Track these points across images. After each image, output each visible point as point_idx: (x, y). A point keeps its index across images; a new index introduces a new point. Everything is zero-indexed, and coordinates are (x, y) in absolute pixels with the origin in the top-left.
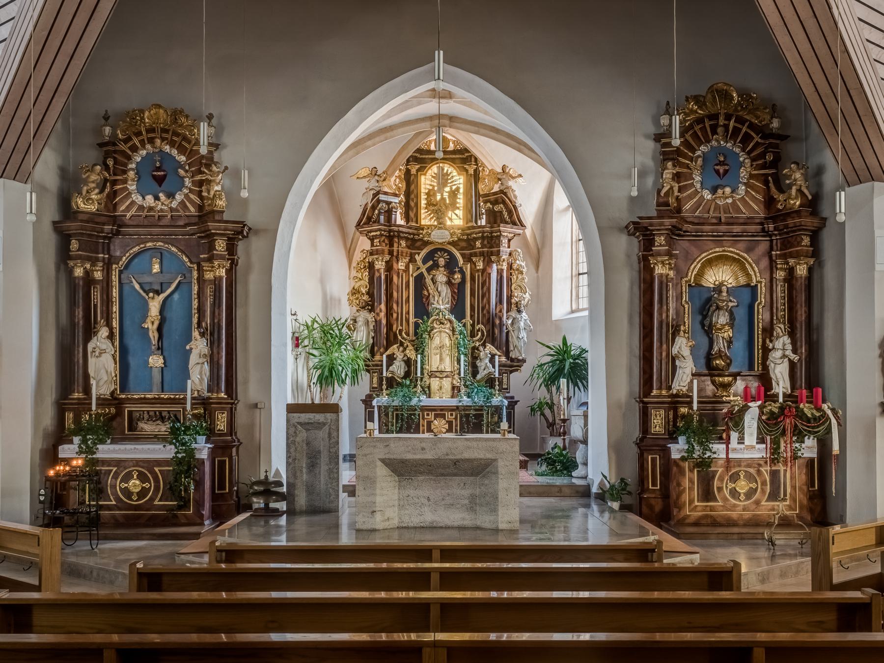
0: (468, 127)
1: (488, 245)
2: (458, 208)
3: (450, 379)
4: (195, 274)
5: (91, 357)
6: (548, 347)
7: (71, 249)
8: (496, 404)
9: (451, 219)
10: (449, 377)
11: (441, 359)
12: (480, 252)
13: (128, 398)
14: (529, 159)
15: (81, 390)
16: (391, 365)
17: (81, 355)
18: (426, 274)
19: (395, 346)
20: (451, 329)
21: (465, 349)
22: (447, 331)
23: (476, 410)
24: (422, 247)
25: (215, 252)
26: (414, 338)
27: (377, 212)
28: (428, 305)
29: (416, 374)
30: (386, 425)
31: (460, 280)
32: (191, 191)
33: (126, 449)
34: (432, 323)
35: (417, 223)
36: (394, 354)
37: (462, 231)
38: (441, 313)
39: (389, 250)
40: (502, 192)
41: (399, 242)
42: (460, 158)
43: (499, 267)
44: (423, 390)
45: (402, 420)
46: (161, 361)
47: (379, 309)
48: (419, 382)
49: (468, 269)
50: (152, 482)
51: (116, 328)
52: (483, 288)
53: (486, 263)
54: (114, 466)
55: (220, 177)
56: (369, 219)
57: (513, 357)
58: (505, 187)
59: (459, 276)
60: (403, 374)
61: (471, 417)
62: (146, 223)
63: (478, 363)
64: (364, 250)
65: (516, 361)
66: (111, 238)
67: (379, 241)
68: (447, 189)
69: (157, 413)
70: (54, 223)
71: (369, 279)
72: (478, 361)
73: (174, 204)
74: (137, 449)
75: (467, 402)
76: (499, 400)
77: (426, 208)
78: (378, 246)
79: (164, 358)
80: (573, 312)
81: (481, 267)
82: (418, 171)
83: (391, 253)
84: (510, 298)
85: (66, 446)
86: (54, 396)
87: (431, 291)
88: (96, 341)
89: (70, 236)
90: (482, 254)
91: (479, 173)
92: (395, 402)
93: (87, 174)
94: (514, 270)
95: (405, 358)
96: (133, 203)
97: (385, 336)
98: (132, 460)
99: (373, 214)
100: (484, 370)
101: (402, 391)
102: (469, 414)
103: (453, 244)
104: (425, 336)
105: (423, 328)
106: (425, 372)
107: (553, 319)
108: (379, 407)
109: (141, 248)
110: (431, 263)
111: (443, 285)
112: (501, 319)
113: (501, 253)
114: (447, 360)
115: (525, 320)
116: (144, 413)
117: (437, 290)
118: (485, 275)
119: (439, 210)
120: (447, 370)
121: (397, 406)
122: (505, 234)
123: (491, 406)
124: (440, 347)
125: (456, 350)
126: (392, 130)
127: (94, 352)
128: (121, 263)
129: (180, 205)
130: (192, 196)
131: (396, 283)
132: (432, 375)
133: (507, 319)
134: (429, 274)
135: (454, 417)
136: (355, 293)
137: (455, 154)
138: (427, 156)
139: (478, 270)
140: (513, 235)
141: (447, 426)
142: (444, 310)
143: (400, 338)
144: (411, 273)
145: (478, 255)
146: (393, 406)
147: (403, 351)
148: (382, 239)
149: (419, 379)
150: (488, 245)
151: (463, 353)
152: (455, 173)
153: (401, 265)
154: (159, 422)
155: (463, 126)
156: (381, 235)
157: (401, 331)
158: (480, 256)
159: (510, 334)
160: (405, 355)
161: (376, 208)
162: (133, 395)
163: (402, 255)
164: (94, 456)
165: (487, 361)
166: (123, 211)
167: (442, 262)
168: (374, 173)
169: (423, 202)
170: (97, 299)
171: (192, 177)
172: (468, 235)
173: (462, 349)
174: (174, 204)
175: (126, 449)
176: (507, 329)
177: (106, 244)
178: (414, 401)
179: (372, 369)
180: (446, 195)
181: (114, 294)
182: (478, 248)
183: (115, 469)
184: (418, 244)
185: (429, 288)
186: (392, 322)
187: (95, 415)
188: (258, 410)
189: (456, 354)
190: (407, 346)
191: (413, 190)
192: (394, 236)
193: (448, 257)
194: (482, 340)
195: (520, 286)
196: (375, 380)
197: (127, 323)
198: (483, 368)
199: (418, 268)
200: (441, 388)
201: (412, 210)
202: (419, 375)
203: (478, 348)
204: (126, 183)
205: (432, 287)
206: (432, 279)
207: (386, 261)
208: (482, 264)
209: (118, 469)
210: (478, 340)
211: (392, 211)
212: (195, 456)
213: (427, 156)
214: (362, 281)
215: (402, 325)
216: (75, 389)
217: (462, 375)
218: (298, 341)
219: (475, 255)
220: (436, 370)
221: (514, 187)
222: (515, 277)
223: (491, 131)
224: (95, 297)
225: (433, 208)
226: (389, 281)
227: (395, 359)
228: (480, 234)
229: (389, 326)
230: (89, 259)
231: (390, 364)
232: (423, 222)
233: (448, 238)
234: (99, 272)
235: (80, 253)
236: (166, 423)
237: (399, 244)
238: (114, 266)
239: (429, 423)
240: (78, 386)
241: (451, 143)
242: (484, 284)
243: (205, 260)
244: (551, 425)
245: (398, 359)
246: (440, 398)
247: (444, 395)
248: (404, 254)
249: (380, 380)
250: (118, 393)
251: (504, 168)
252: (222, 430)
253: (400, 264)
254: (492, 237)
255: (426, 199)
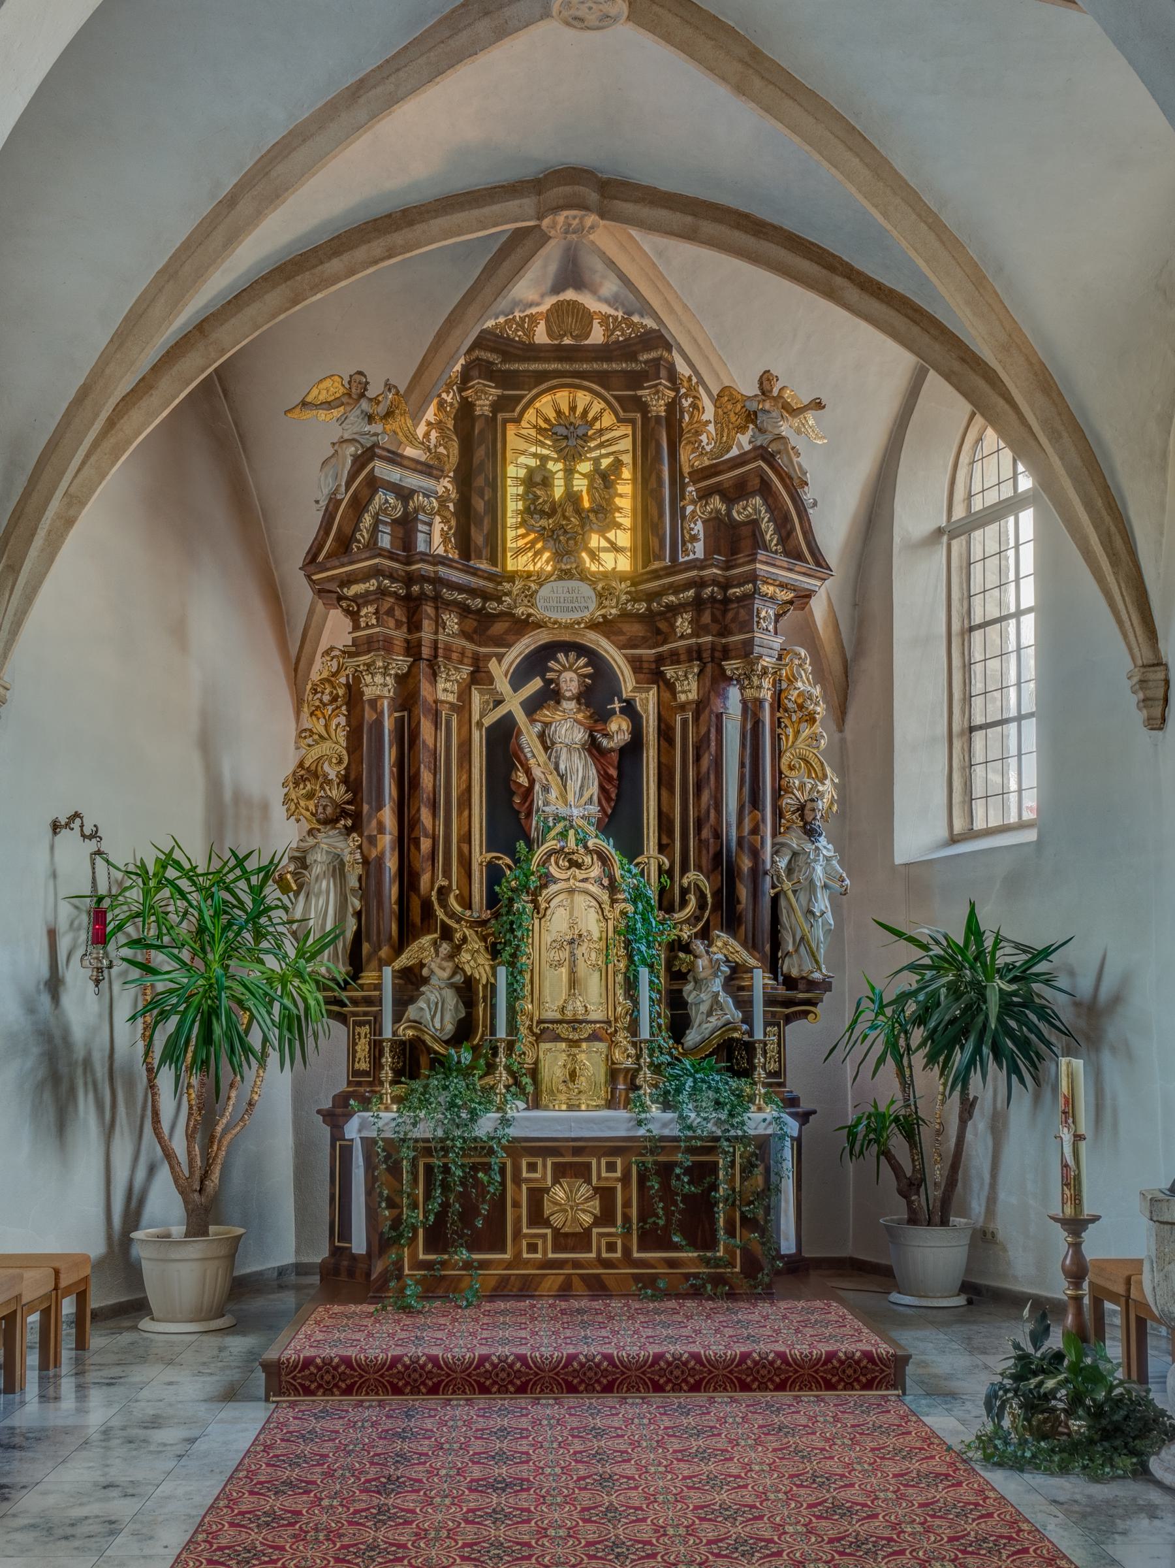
0: (662, 214)
1: (715, 628)
2: (619, 526)
3: (602, 1046)
6: (911, 940)
8: (761, 1131)
9: (593, 556)
10: (600, 1040)
11: (573, 982)
12: (689, 650)
14: (863, 325)
16: (412, 1000)
18: (521, 717)
19: (426, 940)
20: (606, 882)
21: (649, 947)
22: (594, 889)
23: (691, 1150)
24: (510, 638)
26: (487, 914)
27: (367, 520)
28: (529, 814)
29: (493, 1032)
30: (392, 1204)
31: (627, 737)
34: (544, 863)
35: (495, 564)
36: (422, 965)
37: (633, 584)
38: (571, 832)
39: (407, 641)
40: (762, 453)
41: (438, 616)
42: (624, 372)
43: (749, 693)
44: (517, 1083)
45: (446, 1187)
47: (374, 823)
48: (502, 1059)
49: (648, 703)
52: (698, 758)
53: (708, 684)
56: (345, 544)
57: (795, 973)
58: (770, 437)
59: (624, 726)
60: (450, 1027)
61: (678, 1177)
63: (689, 992)
64: (332, 649)
65: (801, 986)
67: (377, 612)
68: (585, 467)
71: (348, 738)
72: (689, 987)
75: (665, 1125)
76: (769, 1118)
77: (523, 523)
78: (373, 626)
80: (954, 840)
81: (693, 696)
82: (497, 407)
83: (412, 649)
84: (779, 792)
87: (537, 772)
90: (695, 654)
91: (682, 417)
92: (421, 1126)
94: (786, 710)
95: (458, 978)
97: (395, 907)
99: (356, 528)
100: (710, 1013)
101: (445, 1088)
102: (674, 1164)
103: (604, 626)
104: (522, 903)
105: (516, 878)
106: (523, 1023)
107: (899, 860)
108: (368, 1143)
110: (536, 684)
111: (576, 756)
112: (755, 854)
113: (757, 649)
114: (593, 985)
115: (828, 859)
117: (557, 768)
118: (704, 717)
119: (562, 527)
120: (593, 1016)
121: (427, 1140)
122: (769, 590)
123: (744, 1139)
124: (572, 942)
125: (622, 952)
126: (411, 223)
131: (430, 742)
132: (544, 1032)
133: (776, 853)
134: (533, 721)
135: (619, 1174)
136: (303, 779)
137: (609, 359)
138: (522, 367)
139: (683, 707)
140: (791, 595)
141: (595, 1205)
142: (581, 822)
143: (440, 913)
144: (476, 717)
145: (683, 657)
146: (416, 1140)
147: (451, 957)
148: (386, 606)
149: (502, 1047)
150: (715, 628)
151: (644, 962)
152: (608, 419)
153: (445, 690)
155: (645, 212)
156: (382, 592)
157: (443, 892)
158: (690, 660)
159: (783, 903)
160: (458, 969)
161: (364, 509)
163: (448, 658)
165: (717, 985)
167: (570, 683)
168: (356, 389)
169: (513, 506)
172: (651, 597)
173: (643, 948)
176: (774, 887)
178: (486, 1125)
179: (354, 1014)
180: (580, 484)
182: (682, 637)
184: (498, 628)
185: (532, 761)
186: (417, 865)
189: (622, 965)
190: (464, 940)
191: (482, 463)
192: (422, 597)
193: (589, 670)
194: (698, 919)
195: (807, 762)
196: (363, 1048)
198: (704, 1008)
199: (498, 703)
200: (573, 1075)
201: (479, 524)
202: (502, 1033)
203: (688, 944)
205: (542, 757)
206: (542, 736)
207: (397, 675)
208: (694, 686)
210: (687, 921)
211: (416, 519)
213: (522, 367)
214: (328, 744)
215: (447, 874)
217: (645, 1034)
218: (105, 925)
219: (674, 658)
220: (558, 1016)
221: (794, 440)
222: (790, 731)
223: (738, 227)
225: (544, 522)
226: (407, 737)
227: (425, 981)
228: (691, 593)
229: (408, 877)
231: (402, 1002)
232: (511, 566)
233: (591, 610)
237: (439, 624)
239: (537, 1196)
241: (596, 322)
242: (700, 749)
244: (910, 1186)
245: (434, 981)
246: (571, 1108)
247: (583, 1097)
248: (455, 656)
249: (376, 1048)
251: (766, 380)
253: (441, 685)
254: (726, 601)
255: (523, 497)
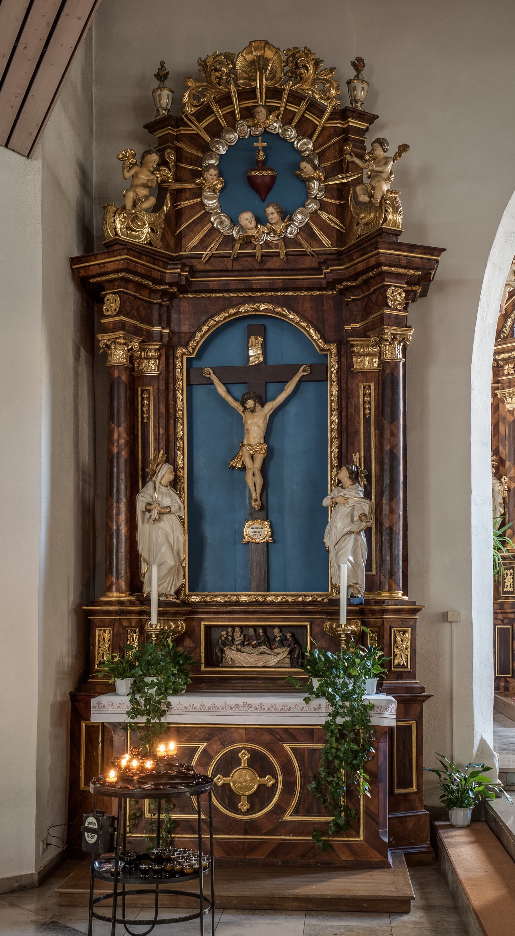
4: (333, 363)
5: (143, 522)
7: (105, 313)
13: (205, 602)
15: (123, 584)
17: (123, 517)
25: (386, 311)
32: (323, 206)
33: (226, 705)
46: (267, 531)
50: (279, 773)
51: (183, 468)
54: (202, 741)
55: (389, 168)
62: (237, 266)
66: (172, 297)
69: (261, 631)
70: (73, 261)
73: (292, 231)
74: (250, 706)
79: (271, 526)
85: (105, 699)
86: (72, 598)
88: (152, 490)
89: (101, 287)
93: (133, 172)
96: (213, 230)
98: (237, 728)
109: (231, 315)
116: (234, 631)
127: (149, 511)
128: (192, 344)
129: (302, 233)
130: (325, 216)
154: (263, 648)
162: (215, 596)
164: (163, 720)
166: (195, 248)
170: (148, 411)
171: (326, 178)
174: (292, 231)
175: (226, 705)
177: (165, 308)
181: (179, 404)
183: (202, 746)
187: (157, 636)
188: (447, 626)
197: (200, 462)
204: (200, 195)
209: (209, 746)
212: (369, 721)
216: (111, 585)
224: (145, 409)
230: (137, 332)
234: (153, 361)
235: (122, 318)
236: (276, 651)
238: (180, 351)
240: (117, 578)
243: (355, 333)
250: (187, 592)
252: (403, 666)
